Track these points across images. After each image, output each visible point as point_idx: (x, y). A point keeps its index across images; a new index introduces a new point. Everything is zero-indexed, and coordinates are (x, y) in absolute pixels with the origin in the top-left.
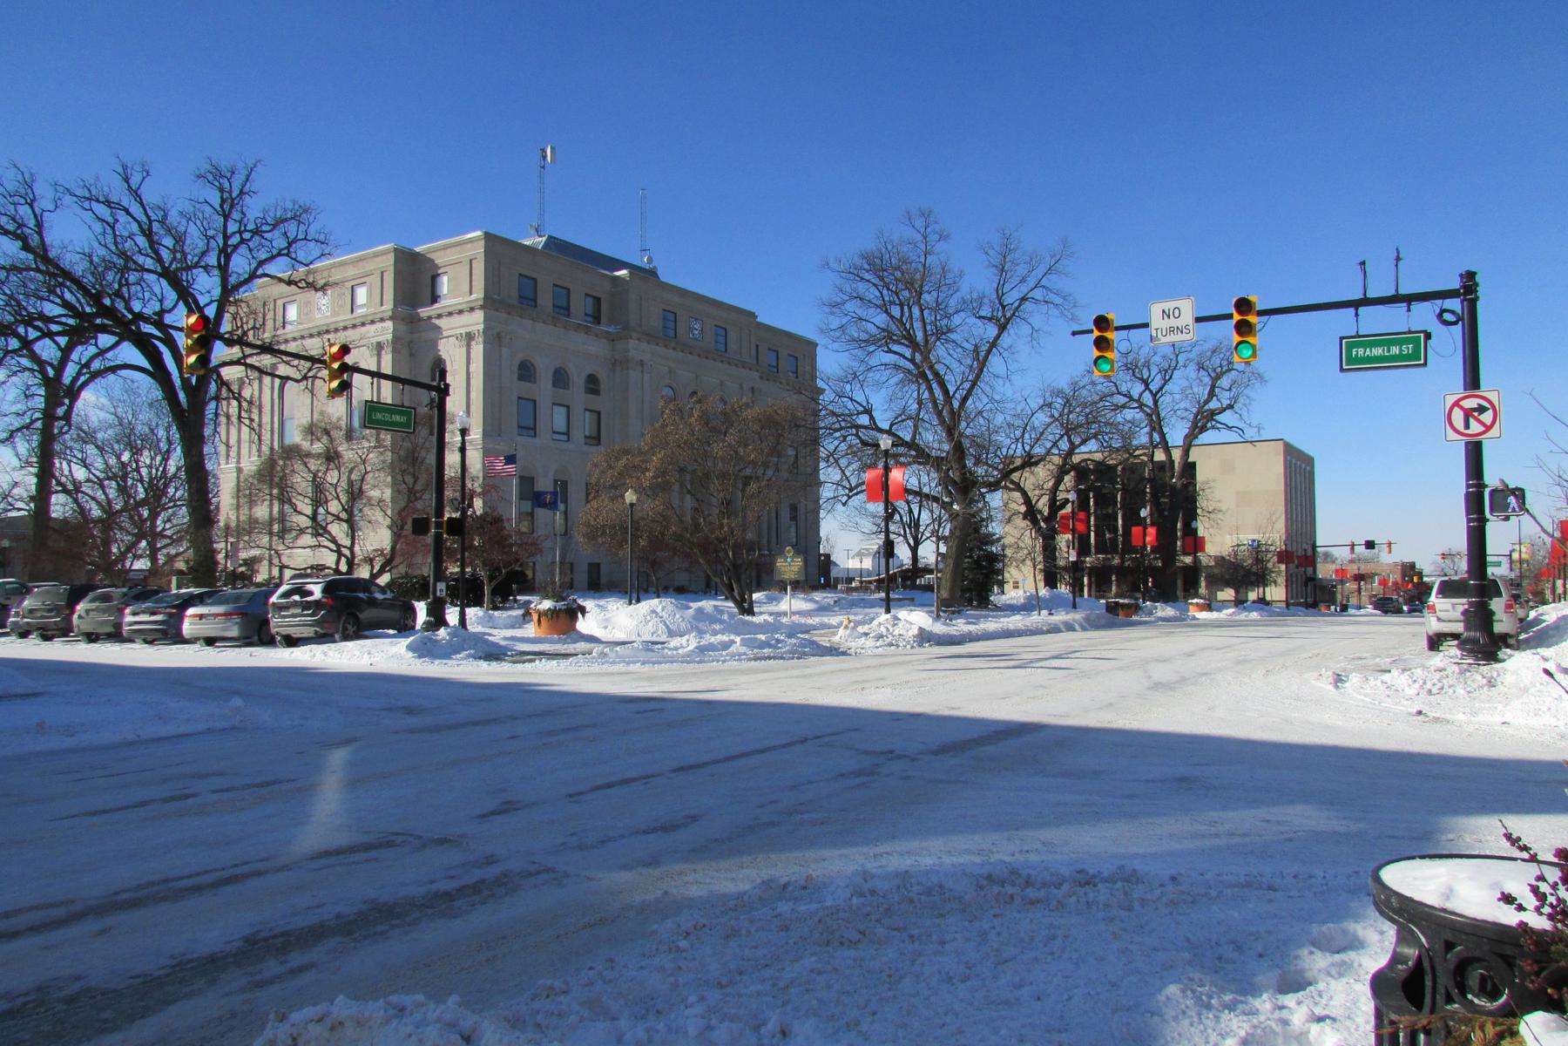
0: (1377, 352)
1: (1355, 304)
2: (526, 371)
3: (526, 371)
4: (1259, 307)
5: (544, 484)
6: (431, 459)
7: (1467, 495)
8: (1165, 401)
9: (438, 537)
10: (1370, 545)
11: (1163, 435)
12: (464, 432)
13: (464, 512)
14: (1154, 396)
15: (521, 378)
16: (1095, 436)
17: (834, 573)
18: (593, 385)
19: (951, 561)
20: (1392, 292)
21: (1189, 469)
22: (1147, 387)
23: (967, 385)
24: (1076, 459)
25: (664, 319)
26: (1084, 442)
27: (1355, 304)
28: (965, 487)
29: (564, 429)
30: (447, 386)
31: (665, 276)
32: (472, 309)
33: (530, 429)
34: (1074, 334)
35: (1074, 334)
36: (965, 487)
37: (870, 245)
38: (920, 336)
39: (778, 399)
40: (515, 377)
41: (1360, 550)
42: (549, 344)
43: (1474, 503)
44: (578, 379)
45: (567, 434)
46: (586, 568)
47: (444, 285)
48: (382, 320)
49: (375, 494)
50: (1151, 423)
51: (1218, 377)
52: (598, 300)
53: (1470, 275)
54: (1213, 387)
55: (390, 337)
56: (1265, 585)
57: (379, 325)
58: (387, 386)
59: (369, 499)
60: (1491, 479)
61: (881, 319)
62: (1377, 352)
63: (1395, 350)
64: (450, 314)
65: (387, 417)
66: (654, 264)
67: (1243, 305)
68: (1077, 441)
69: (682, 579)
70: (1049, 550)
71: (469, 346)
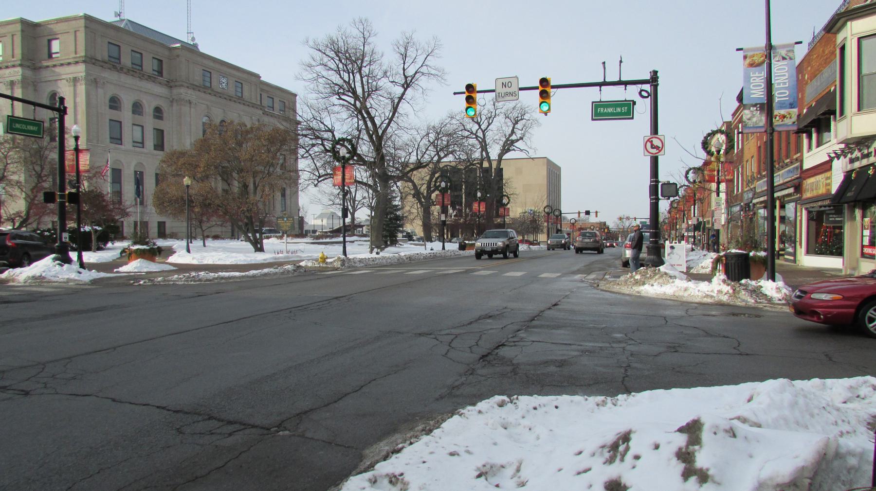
0: (610, 110)
1: (600, 85)
2: (115, 103)
3: (115, 103)
4: (552, 84)
5: (524, 474)
6: (54, 156)
7: (650, 186)
8: (489, 134)
9: (62, 205)
10: (588, 213)
11: (487, 153)
12: (77, 138)
13: (78, 190)
14: (483, 132)
15: (111, 107)
16: (452, 153)
17: (306, 228)
18: (158, 113)
19: (376, 220)
20: (617, 79)
21: (500, 171)
22: (480, 126)
23: (387, 121)
24: (441, 165)
25: (204, 75)
26: (446, 156)
27: (600, 85)
28: (385, 178)
29: (140, 141)
30: (65, 108)
31: (202, 49)
32: (77, 63)
33: (117, 139)
34: (455, 94)
35: (455, 94)
36: (385, 178)
37: (334, 34)
38: (359, 91)
39: (273, 123)
40: (108, 108)
41: (583, 215)
42: (129, 90)
43: (654, 190)
44: (149, 109)
45: (143, 143)
46: (156, 225)
47: (56, 46)
48: (14, 66)
49: (15, 178)
50: (482, 147)
51: (517, 123)
52: (161, 61)
53: (655, 72)
54: (514, 128)
55: (20, 78)
56: (537, 233)
57: (11, 70)
58: (18, 105)
59: (10, 181)
60: (662, 178)
61: (336, 79)
62: (610, 110)
63: (619, 110)
64: (62, 65)
65: (24, 127)
66: (196, 42)
67: (544, 82)
68: (442, 155)
69: (217, 230)
70: (427, 213)
71: (75, 86)
